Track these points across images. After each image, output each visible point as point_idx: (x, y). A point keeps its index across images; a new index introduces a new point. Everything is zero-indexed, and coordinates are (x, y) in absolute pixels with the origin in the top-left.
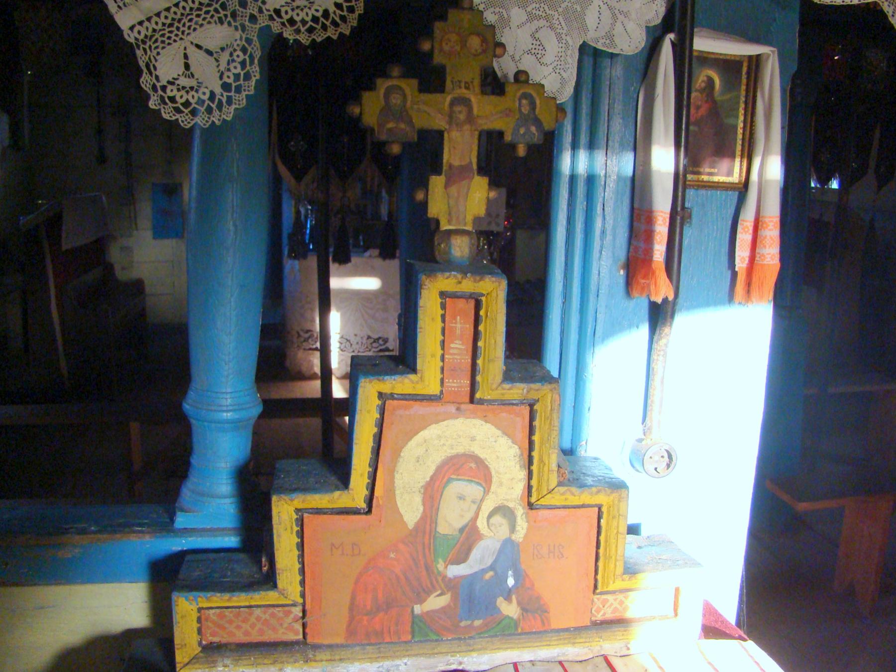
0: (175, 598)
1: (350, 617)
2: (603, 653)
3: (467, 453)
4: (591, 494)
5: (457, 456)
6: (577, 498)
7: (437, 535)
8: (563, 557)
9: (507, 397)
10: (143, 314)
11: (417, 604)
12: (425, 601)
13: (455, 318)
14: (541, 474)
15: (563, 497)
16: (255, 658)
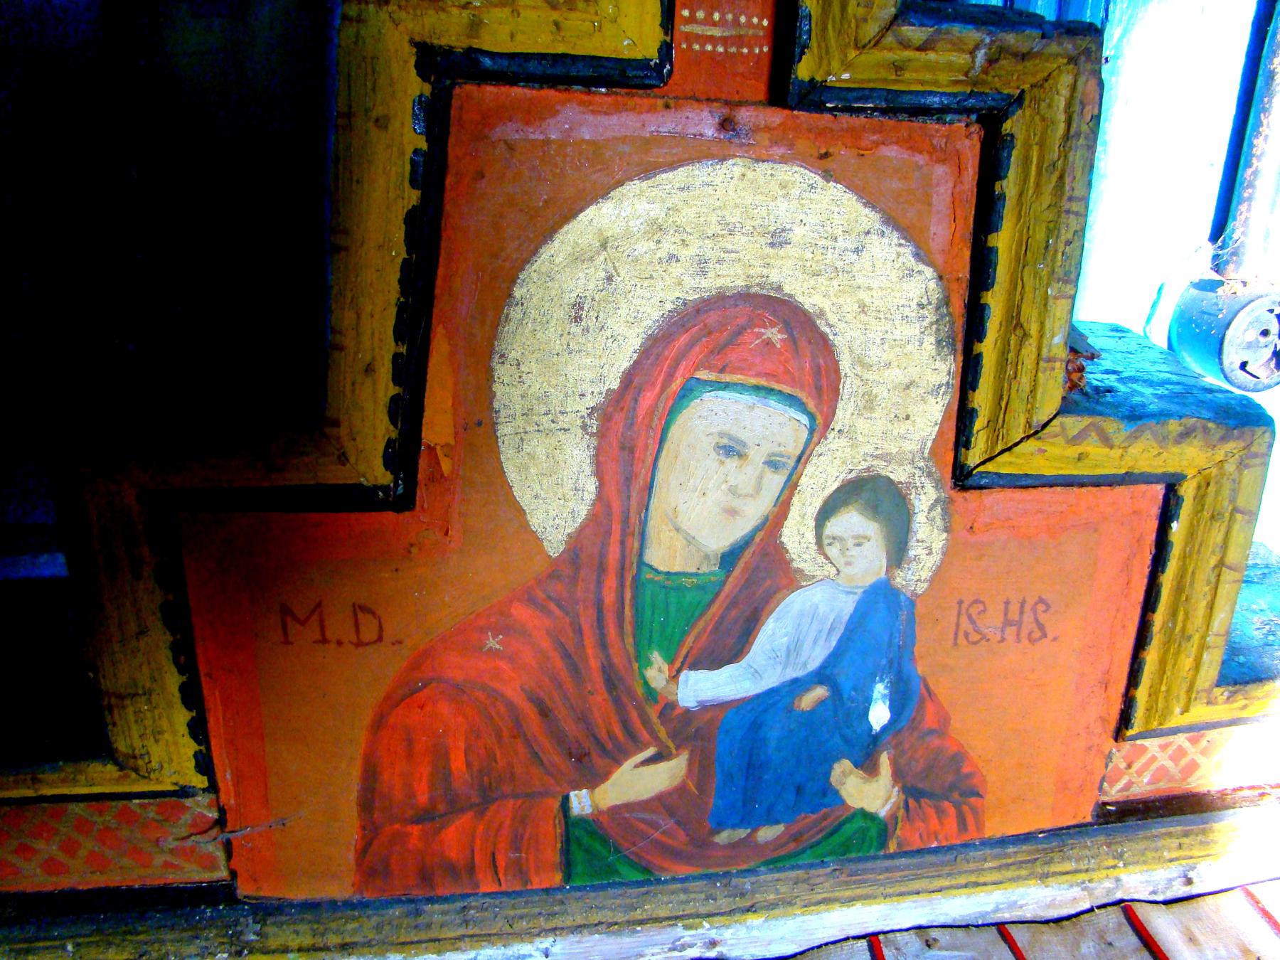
1: (363, 828)
2: (1119, 895)
4: (1163, 440)
5: (720, 300)
6: (1116, 453)
8: (1045, 635)
9: (911, 82)
11: (579, 788)
12: (605, 777)
14: (1010, 372)
15: (1073, 451)
16: (77, 945)
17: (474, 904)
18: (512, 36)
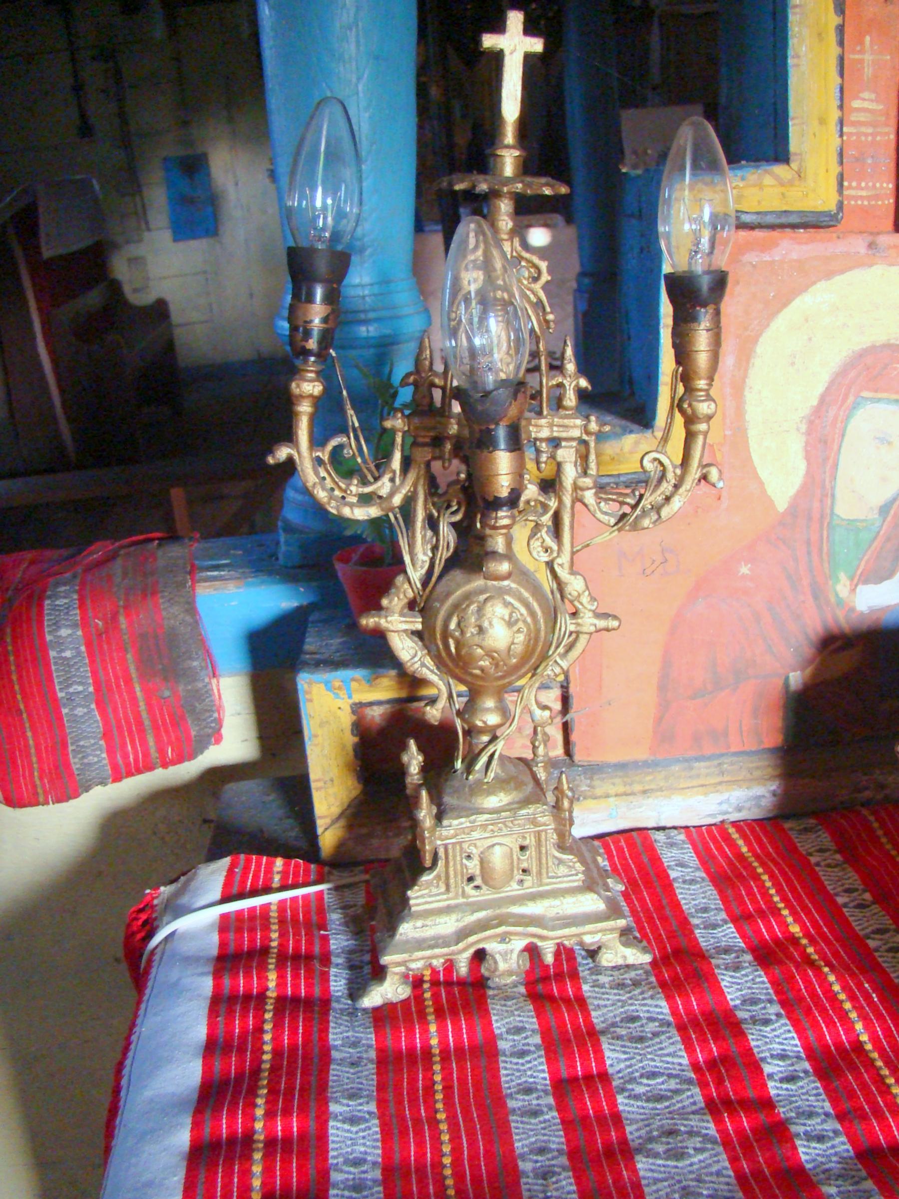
0: (306, 686)
3: (892, 341)
5: (872, 350)
7: (836, 521)
10: (170, 346)
13: (861, 43)
17: (726, 761)
18: (759, 202)
